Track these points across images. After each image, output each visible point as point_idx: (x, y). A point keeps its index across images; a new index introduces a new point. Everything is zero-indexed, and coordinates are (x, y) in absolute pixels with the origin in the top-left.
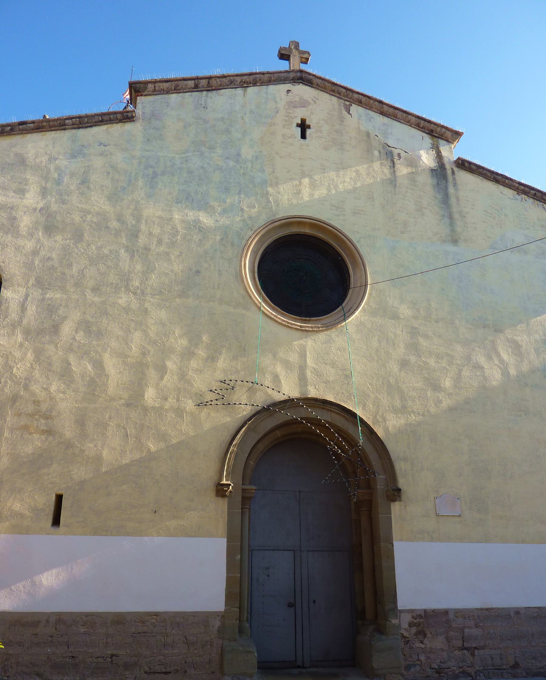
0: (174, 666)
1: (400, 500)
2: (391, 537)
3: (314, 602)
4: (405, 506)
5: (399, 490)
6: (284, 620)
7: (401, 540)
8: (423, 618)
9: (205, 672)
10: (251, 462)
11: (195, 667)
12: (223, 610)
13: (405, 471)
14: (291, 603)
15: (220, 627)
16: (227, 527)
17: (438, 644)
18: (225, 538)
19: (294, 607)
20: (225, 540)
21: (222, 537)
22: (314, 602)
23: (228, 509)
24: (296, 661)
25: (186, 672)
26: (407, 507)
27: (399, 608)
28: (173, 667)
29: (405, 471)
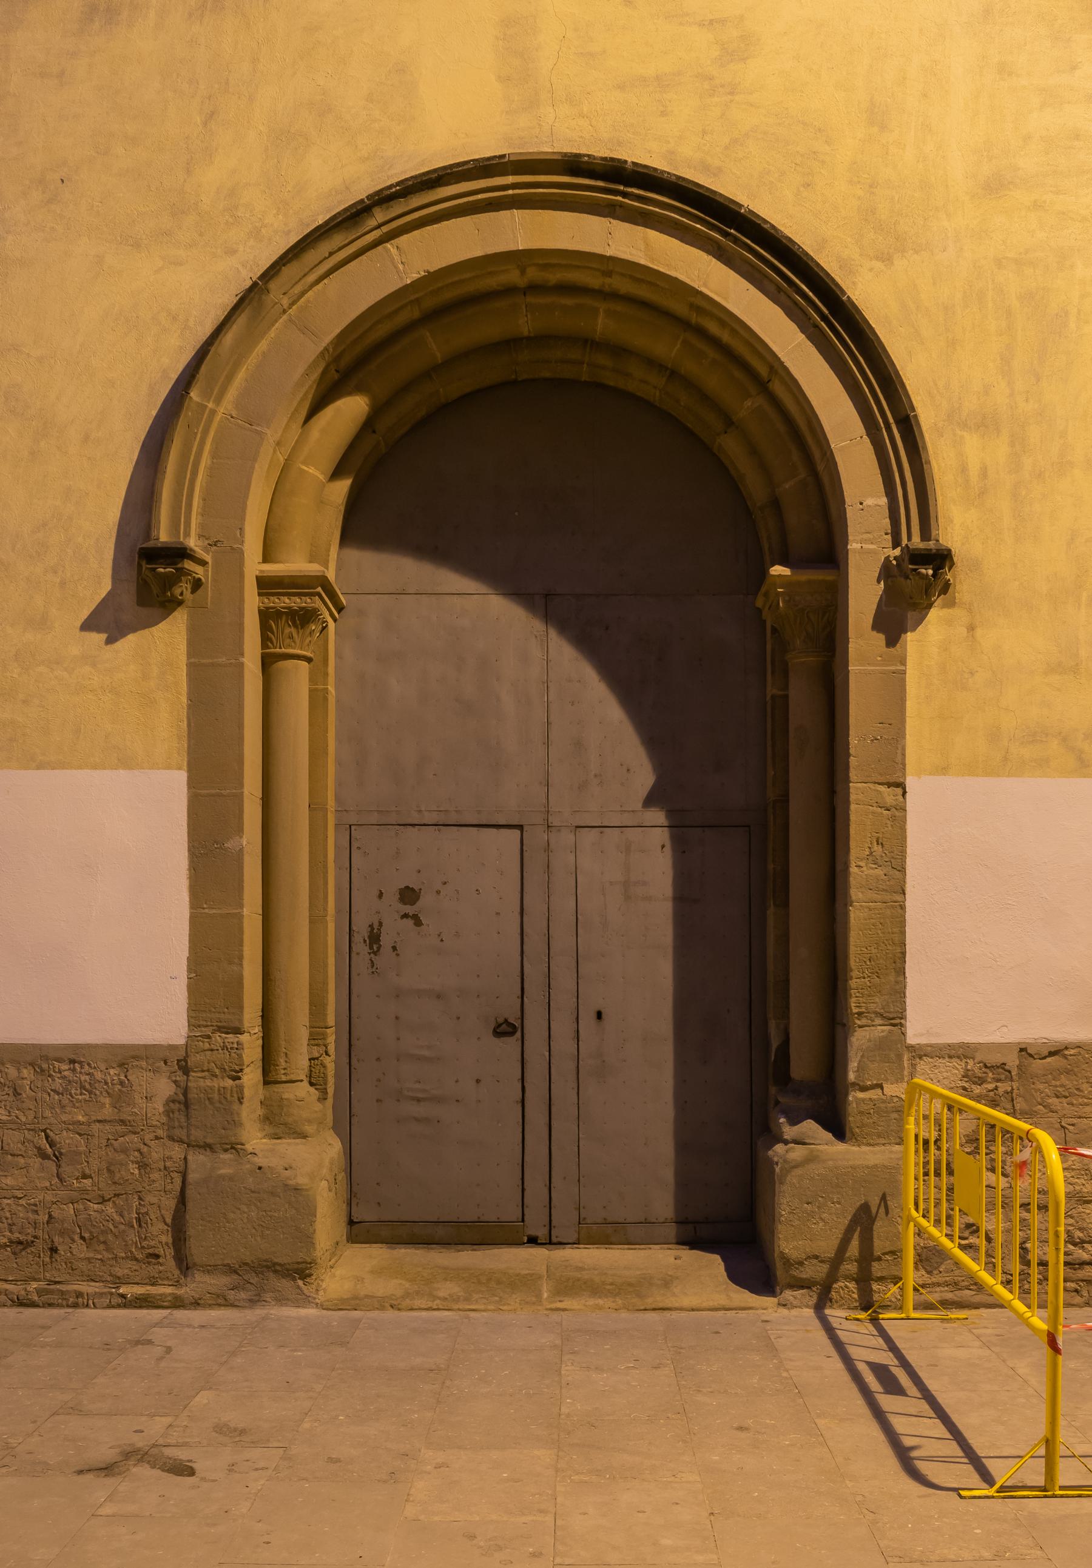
0: (11, 1231)
1: (951, 604)
2: (899, 758)
3: (599, 1015)
4: (971, 628)
5: (941, 559)
6: (478, 1081)
7: (943, 770)
8: (1012, 1080)
9: (123, 1255)
10: (312, 470)
11: (87, 1235)
12: (182, 1041)
13: (984, 473)
14: (506, 1021)
15: (173, 1101)
16: (189, 725)
17: (80, 1118)
18: (180, 769)
19: (518, 1034)
20: (179, 778)
21: (168, 767)
22: (599, 1015)
23: (190, 655)
24: (523, 1221)
25: (54, 1250)
26: (979, 632)
27: (912, 1039)
28: (8, 1233)
29: (984, 473)
